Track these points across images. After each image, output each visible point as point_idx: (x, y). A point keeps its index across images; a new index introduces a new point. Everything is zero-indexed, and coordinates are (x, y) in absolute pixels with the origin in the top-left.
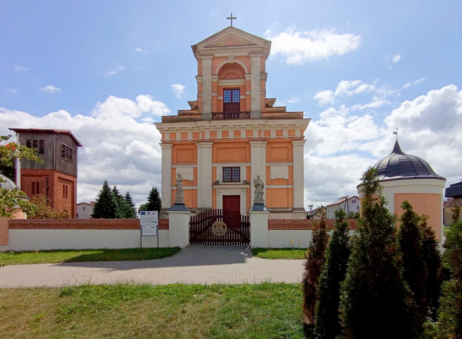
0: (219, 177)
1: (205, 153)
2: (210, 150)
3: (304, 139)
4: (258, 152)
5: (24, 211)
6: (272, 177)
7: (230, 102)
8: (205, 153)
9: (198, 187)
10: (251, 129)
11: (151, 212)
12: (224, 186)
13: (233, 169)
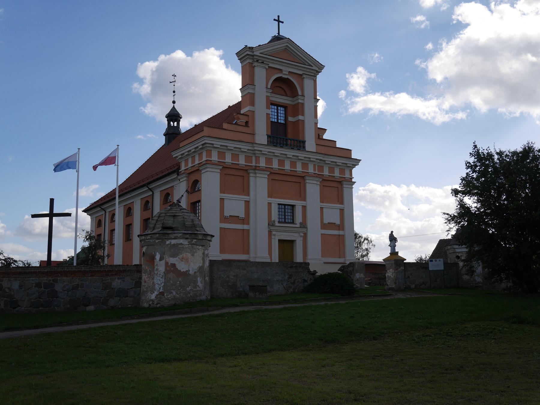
0: (275, 216)
1: (259, 184)
2: (266, 181)
4: (313, 189)
5: (186, 274)
6: (227, 213)
7: (276, 121)
8: (259, 184)
9: (251, 227)
11: (438, 260)
12: (280, 229)
13: (286, 207)
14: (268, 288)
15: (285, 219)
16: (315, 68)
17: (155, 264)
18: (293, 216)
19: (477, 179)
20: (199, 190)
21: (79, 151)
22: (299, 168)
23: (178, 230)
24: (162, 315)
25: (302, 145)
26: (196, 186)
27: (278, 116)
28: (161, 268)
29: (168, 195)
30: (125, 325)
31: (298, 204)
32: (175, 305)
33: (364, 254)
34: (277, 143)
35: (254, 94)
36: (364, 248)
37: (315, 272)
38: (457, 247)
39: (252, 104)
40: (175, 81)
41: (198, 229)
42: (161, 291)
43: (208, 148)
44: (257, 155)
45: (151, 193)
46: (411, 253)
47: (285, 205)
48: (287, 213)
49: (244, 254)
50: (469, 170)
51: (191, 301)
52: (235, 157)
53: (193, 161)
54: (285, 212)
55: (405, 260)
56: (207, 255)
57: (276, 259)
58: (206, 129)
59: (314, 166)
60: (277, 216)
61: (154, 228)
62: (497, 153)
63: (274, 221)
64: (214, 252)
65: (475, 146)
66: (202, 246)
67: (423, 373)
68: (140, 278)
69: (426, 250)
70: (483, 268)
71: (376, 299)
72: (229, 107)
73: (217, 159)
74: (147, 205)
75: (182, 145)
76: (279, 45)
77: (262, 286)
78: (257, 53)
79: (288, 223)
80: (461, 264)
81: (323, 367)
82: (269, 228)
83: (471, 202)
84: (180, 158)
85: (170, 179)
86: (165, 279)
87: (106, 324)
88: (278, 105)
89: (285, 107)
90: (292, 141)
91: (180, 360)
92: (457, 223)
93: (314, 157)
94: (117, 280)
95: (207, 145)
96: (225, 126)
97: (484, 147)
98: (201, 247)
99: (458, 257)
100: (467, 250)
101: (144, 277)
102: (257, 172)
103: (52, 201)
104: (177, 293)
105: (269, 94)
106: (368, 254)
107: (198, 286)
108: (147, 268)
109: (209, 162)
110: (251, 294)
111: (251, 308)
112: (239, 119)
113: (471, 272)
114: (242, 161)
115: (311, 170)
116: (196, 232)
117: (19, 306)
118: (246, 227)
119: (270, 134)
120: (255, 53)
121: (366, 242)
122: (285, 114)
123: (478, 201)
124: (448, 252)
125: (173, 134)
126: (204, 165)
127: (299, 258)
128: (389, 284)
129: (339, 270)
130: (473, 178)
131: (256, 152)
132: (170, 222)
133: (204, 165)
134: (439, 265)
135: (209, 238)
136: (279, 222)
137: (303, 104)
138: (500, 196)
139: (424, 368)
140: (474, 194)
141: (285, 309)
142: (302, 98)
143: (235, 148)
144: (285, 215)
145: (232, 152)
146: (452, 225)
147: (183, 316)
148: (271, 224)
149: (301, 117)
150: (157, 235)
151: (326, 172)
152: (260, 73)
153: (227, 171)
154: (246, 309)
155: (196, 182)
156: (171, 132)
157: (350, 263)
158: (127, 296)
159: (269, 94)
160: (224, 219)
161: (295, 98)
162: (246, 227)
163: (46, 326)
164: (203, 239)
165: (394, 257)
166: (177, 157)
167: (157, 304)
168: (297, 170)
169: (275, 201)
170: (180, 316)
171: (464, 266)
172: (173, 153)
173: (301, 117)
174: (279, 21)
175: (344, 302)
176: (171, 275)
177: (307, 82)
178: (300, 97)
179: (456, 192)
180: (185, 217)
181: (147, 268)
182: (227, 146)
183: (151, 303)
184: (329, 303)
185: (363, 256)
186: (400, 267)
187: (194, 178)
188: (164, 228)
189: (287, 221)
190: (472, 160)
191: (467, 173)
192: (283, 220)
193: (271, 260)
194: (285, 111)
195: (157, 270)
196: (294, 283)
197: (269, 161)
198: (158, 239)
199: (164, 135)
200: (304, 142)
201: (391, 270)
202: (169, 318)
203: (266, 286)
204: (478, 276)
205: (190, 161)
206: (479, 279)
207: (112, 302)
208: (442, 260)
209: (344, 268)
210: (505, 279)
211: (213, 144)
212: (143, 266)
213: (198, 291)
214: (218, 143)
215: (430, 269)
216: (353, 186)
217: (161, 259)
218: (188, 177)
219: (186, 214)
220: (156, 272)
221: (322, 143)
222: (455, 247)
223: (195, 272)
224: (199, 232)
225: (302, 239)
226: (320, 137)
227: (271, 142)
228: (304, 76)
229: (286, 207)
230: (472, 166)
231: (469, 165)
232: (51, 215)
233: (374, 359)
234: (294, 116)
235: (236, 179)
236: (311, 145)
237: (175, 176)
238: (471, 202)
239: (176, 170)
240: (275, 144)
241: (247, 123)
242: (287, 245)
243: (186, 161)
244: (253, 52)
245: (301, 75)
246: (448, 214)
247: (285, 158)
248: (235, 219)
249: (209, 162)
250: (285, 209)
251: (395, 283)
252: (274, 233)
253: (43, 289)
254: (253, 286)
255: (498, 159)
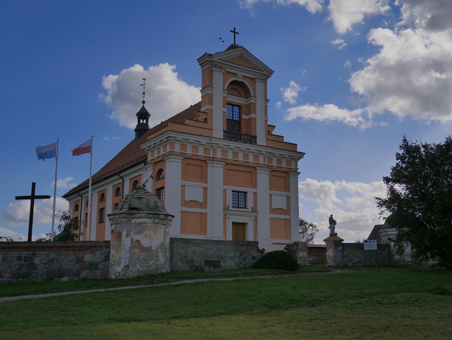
0: (230, 202)
1: (216, 173)
3: (298, 171)
4: (263, 178)
5: (149, 249)
6: (187, 199)
7: (231, 118)
8: (216, 173)
10: (226, 150)
11: (372, 241)
14: (222, 264)
15: (238, 204)
16: (265, 73)
17: (122, 240)
18: (245, 202)
19: (406, 169)
20: (163, 178)
21: (58, 141)
22: (251, 159)
23: (142, 210)
24: (128, 285)
25: (254, 139)
26: (160, 174)
27: (233, 114)
28: (126, 242)
29: (136, 182)
30: (94, 293)
31: (250, 191)
32: (139, 277)
33: (309, 238)
34: (232, 138)
35: (212, 95)
36: (309, 234)
37: (263, 250)
38: (389, 230)
39: (211, 103)
40: (145, 84)
41: (160, 210)
42: (126, 264)
43: (172, 141)
44: (214, 148)
45: (122, 181)
46: (349, 237)
47: (238, 192)
48: (240, 199)
49: (201, 234)
50: (399, 160)
51: (153, 273)
52: (195, 148)
53: (159, 152)
54: (238, 198)
55: (343, 240)
56: (168, 233)
57: (230, 237)
58: (170, 124)
59: (265, 157)
60: (231, 202)
61: (122, 209)
62: (424, 146)
63: (229, 206)
64: (175, 230)
65: (405, 140)
66: (164, 225)
67: (352, 332)
68: (109, 253)
69: (363, 235)
70: (412, 248)
71: (316, 274)
72: (191, 106)
73: (179, 151)
74: (118, 192)
75: (149, 138)
76: (234, 53)
77: (216, 261)
78: (215, 59)
79: (241, 208)
80: (392, 244)
81: (265, 327)
82: (224, 212)
83: (400, 188)
84: (147, 150)
85: (138, 168)
86: (130, 253)
87: (76, 292)
88: (233, 105)
89: (240, 107)
90: (245, 136)
91: (139, 321)
92: (388, 208)
93: (264, 150)
94: (88, 254)
95: (171, 138)
96: (187, 122)
97: (413, 141)
98: (162, 226)
99: (390, 239)
100: (396, 232)
101: (112, 252)
102: (214, 162)
103: (34, 184)
104: (141, 266)
105: (225, 95)
106: (312, 238)
107: (160, 260)
108: (114, 244)
109: (172, 153)
110: (206, 268)
111: (206, 280)
112: (199, 116)
113: (401, 251)
114: (201, 153)
115: (261, 161)
116: (158, 213)
117: (2, 277)
118: (203, 211)
119: (226, 129)
120: (214, 59)
121: (311, 227)
122: (240, 113)
123: (407, 188)
124: (381, 235)
125: (142, 130)
126: (168, 155)
127: (250, 237)
128: (328, 262)
129: (284, 249)
130: (402, 168)
131: (214, 145)
132: (136, 204)
133: (168, 155)
134: (373, 246)
135: (170, 218)
136: (233, 207)
137: (255, 104)
138: (425, 183)
139: (354, 329)
140: (403, 183)
141: (236, 281)
142: (254, 98)
143: (195, 141)
144: (238, 201)
145: (192, 145)
146: (384, 209)
147: (145, 286)
148: (226, 208)
149: (253, 116)
150: (124, 215)
151: (275, 163)
152: (218, 76)
153: (187, 160)
154: (201, 280)
155: (161, 171)
156: (141, 128)
157: (295, 243)
158: (97, 269)
159: (225, 95)
160: (185, 203)
161: (249, 99)
162: (203, 211)
163: (24, 294)
164: (164, 219)
165: (334, 238)
166: (144, 149)
167: (123, 276)
168: (249, 161)
169: (230, 189)
170: (142, 286)
171: (395, 245)
172: (141, 146)
173: (253, 116)
174: (235, 32)
175: (288, 276)
176: (136, 250)
177: (259, 85)
178: (252, 98)
179: (387, 180)
180: (149, 199)
181: (114, 244)
182: (188, 140)
183: (117, 275)
184: (275, 277)
185: (308, 240)
186: (339, 247)
187: (159, 167)
188: (131, 208)
189: (240, 206)
190: (401, 152)
191: (397, 164)
192: (237, 205)
193: (226, 239)
194: (240, 110)
195: (124, 245)
196: (245, 260)
197: (225, 152)
198: (125, 218)
199: (135, 131)
200: (255, 137)
201: (331, 249)
202: (133, 287)
203: (220, 262)
204: (408, 256)
205: (156, 152)
206: (408, 259)
207: (84, 274)
208: (375, 241)
209: (288, 247)
210: (431, 258)
211: (176, 138)
212: (111, 242)
213: (159, 264)
214: (180, 137)
215: (365, 249)
216: (298, 176)
217: (127, 236)
218: (154, 166)
219: (150, 196)
220: (122, 248)
221: (271, 138)
222: (387, 230)
223: (157, 248)
224: (161, 213)
225: (253, 222)
226: (270, 133)
227: (226, 137)
228: (257, 80)
229: (240, 194)
230: (402, 157)
231: (398, 157)
232: (33, 197)
233: (310, 321)
234: (247, 114)
235: (196, 167)
236: (261, 139)
237: (142, 165)
238: (400, 188)
239: (144, 161)
240: (230, 139)
241: (206, 119)
242: (239, 227)
243: (153, 152)
244: (212, 58)
245: (254, 79)
246: (380, 199)
247: (238, 150)
248: (194, 203)
249: (172, 153)
250: (238, 195)
251: (334, 261)
252: (228, 216)
253: (23, 262)
254: (209, 261)
255: (424, 151)
